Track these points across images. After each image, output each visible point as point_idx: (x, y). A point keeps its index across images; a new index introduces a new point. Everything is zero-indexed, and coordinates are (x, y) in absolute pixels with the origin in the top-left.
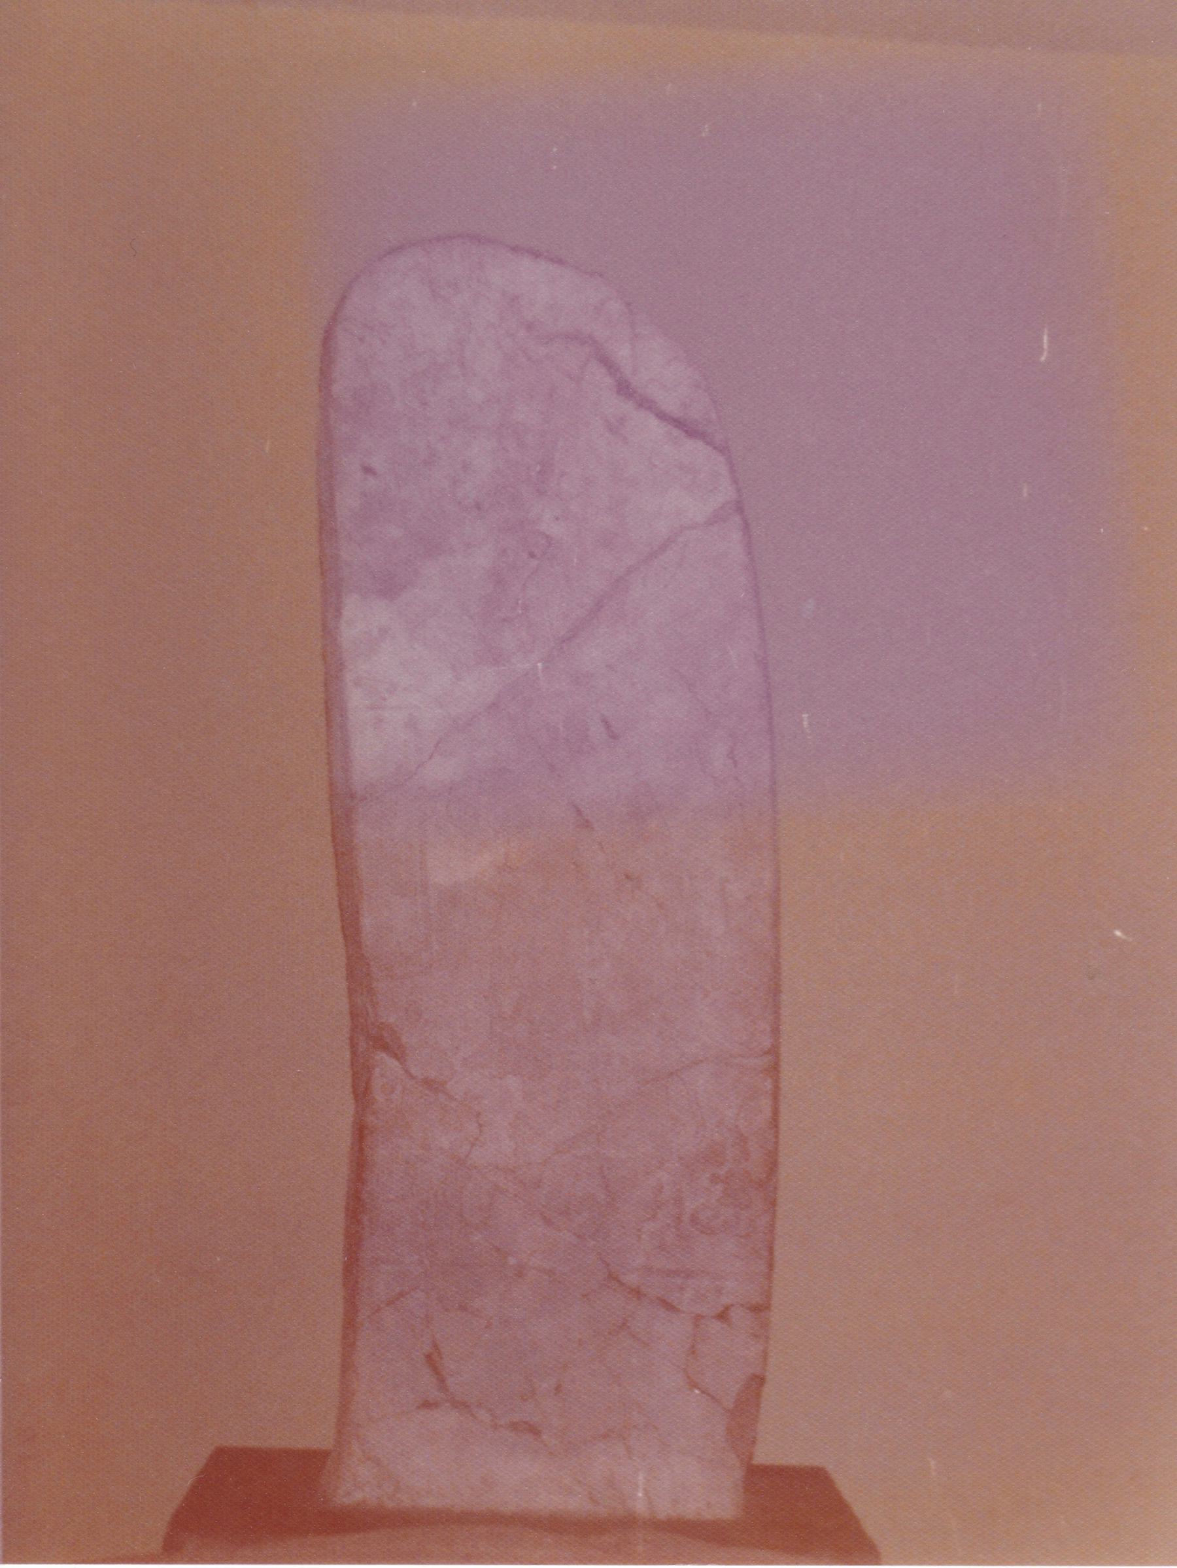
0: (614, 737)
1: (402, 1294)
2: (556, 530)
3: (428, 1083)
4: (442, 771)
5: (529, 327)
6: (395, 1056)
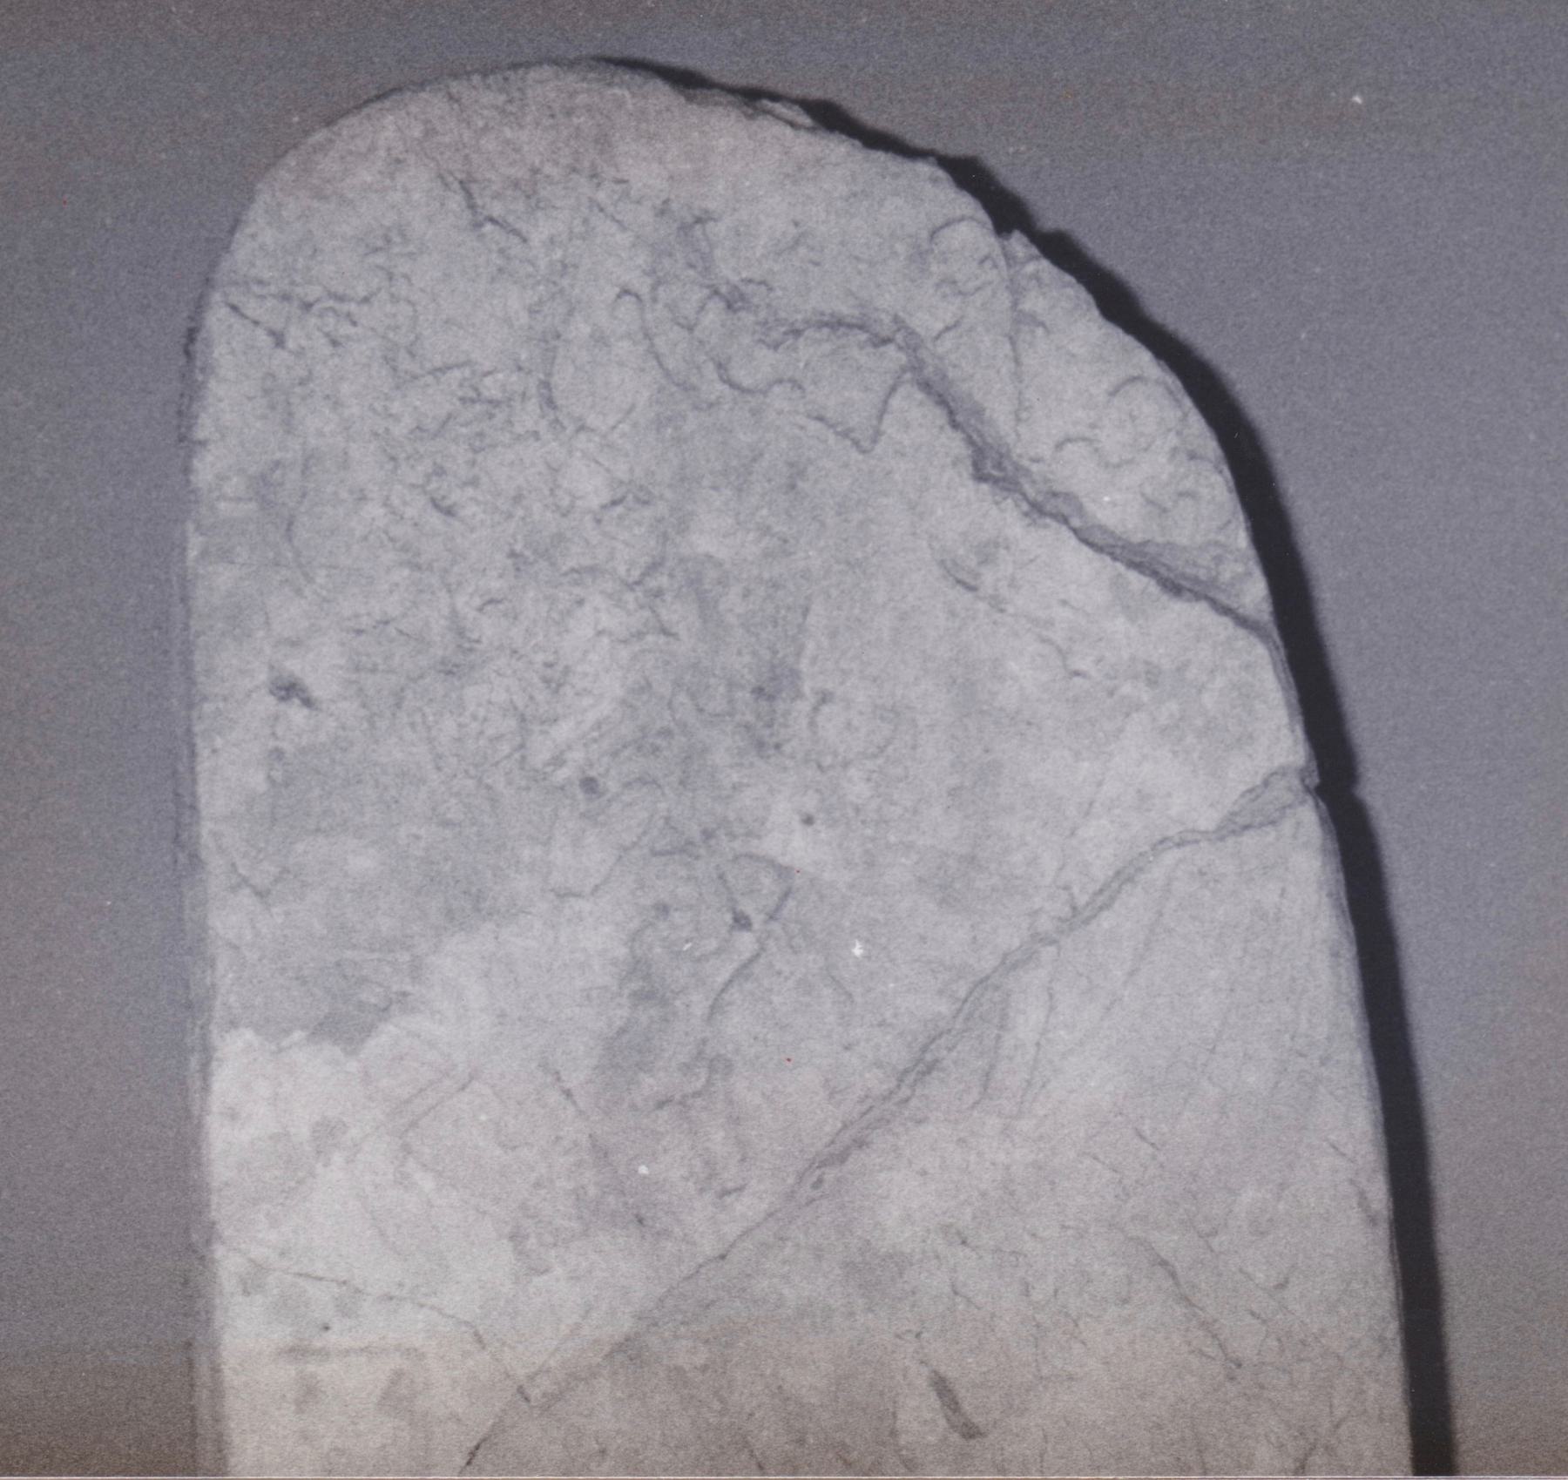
0: (971, 1432)
2: (798, 848)
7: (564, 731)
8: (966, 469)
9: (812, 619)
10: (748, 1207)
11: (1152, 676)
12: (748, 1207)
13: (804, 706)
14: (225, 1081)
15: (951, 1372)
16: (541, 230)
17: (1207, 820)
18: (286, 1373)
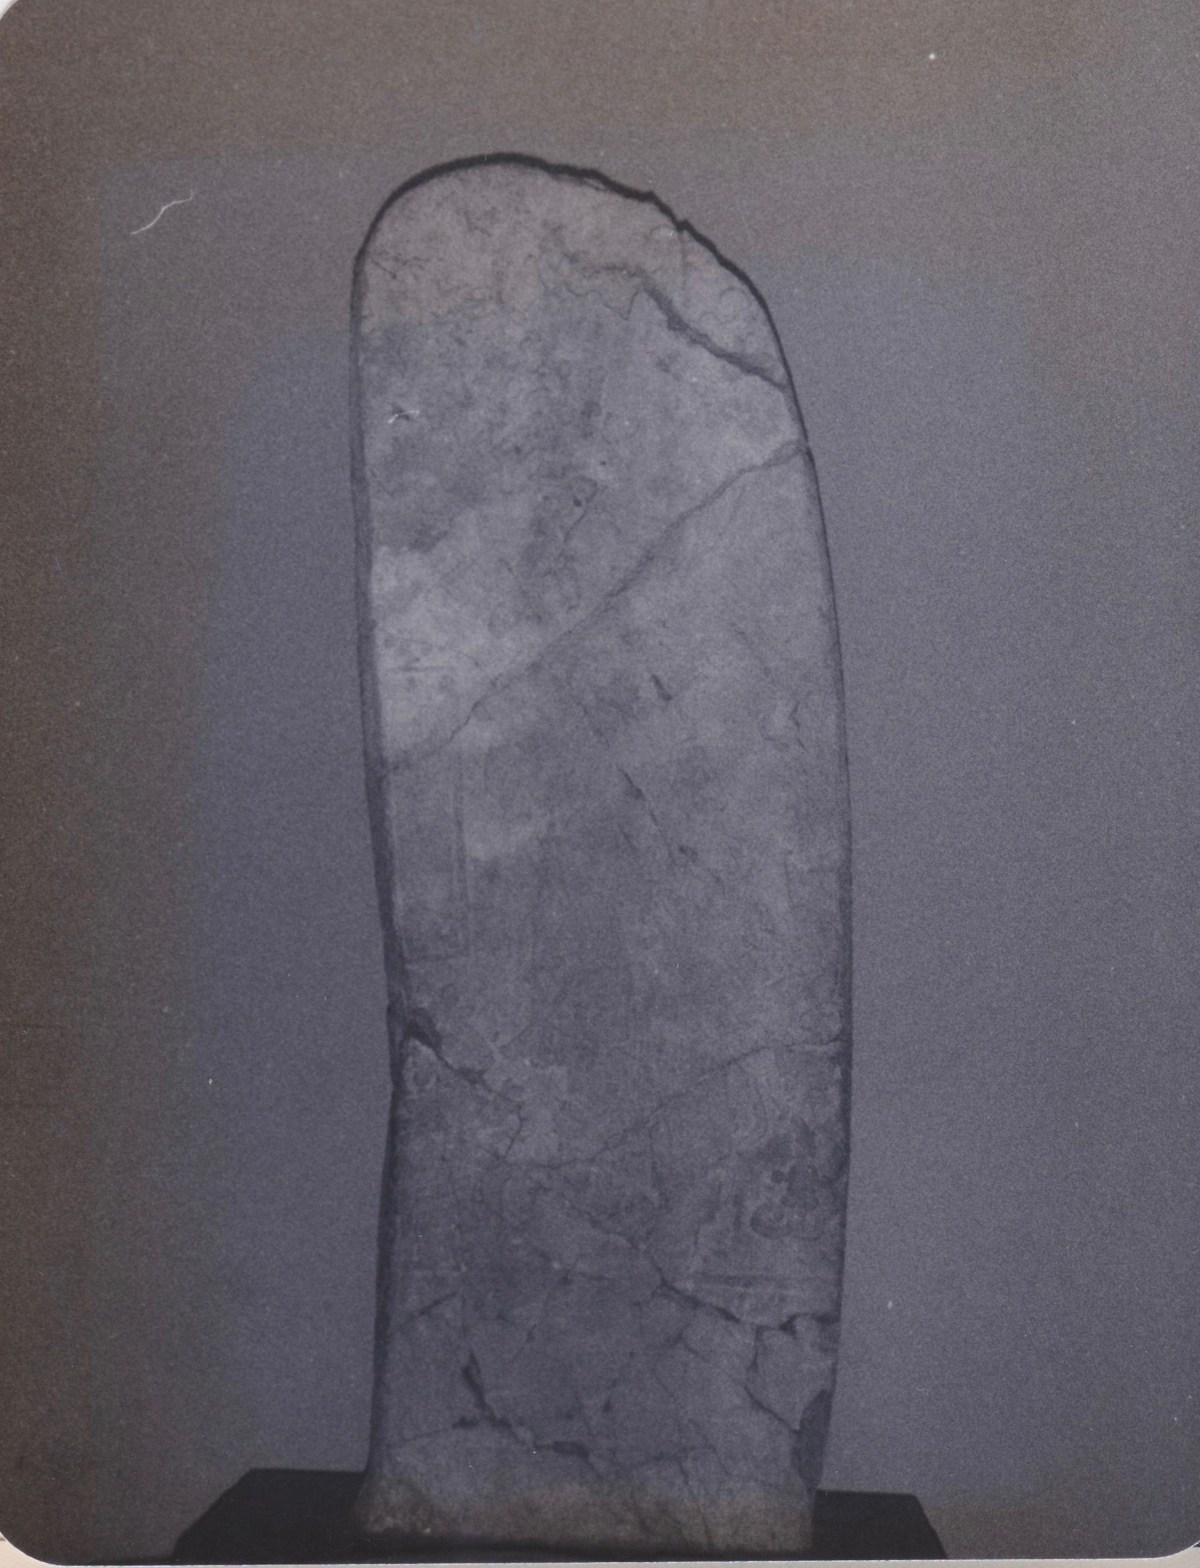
0: (668, 698)
1: (437, 1303)
2: (601, 475)
3: (465, 1073)
4: (480, 735)
5: (573, 259)
6: (429, 1045)
7: (508, 429)
8: (665, 325)
9: (604, 385)
10: (580, 614)
11: (738, 407)
12: (580, 614)
13: (602, 418)
14: (377, 568)
15: (659, 673)
16: (497, 231)
17: (758, 461)
18: (401, 676)
